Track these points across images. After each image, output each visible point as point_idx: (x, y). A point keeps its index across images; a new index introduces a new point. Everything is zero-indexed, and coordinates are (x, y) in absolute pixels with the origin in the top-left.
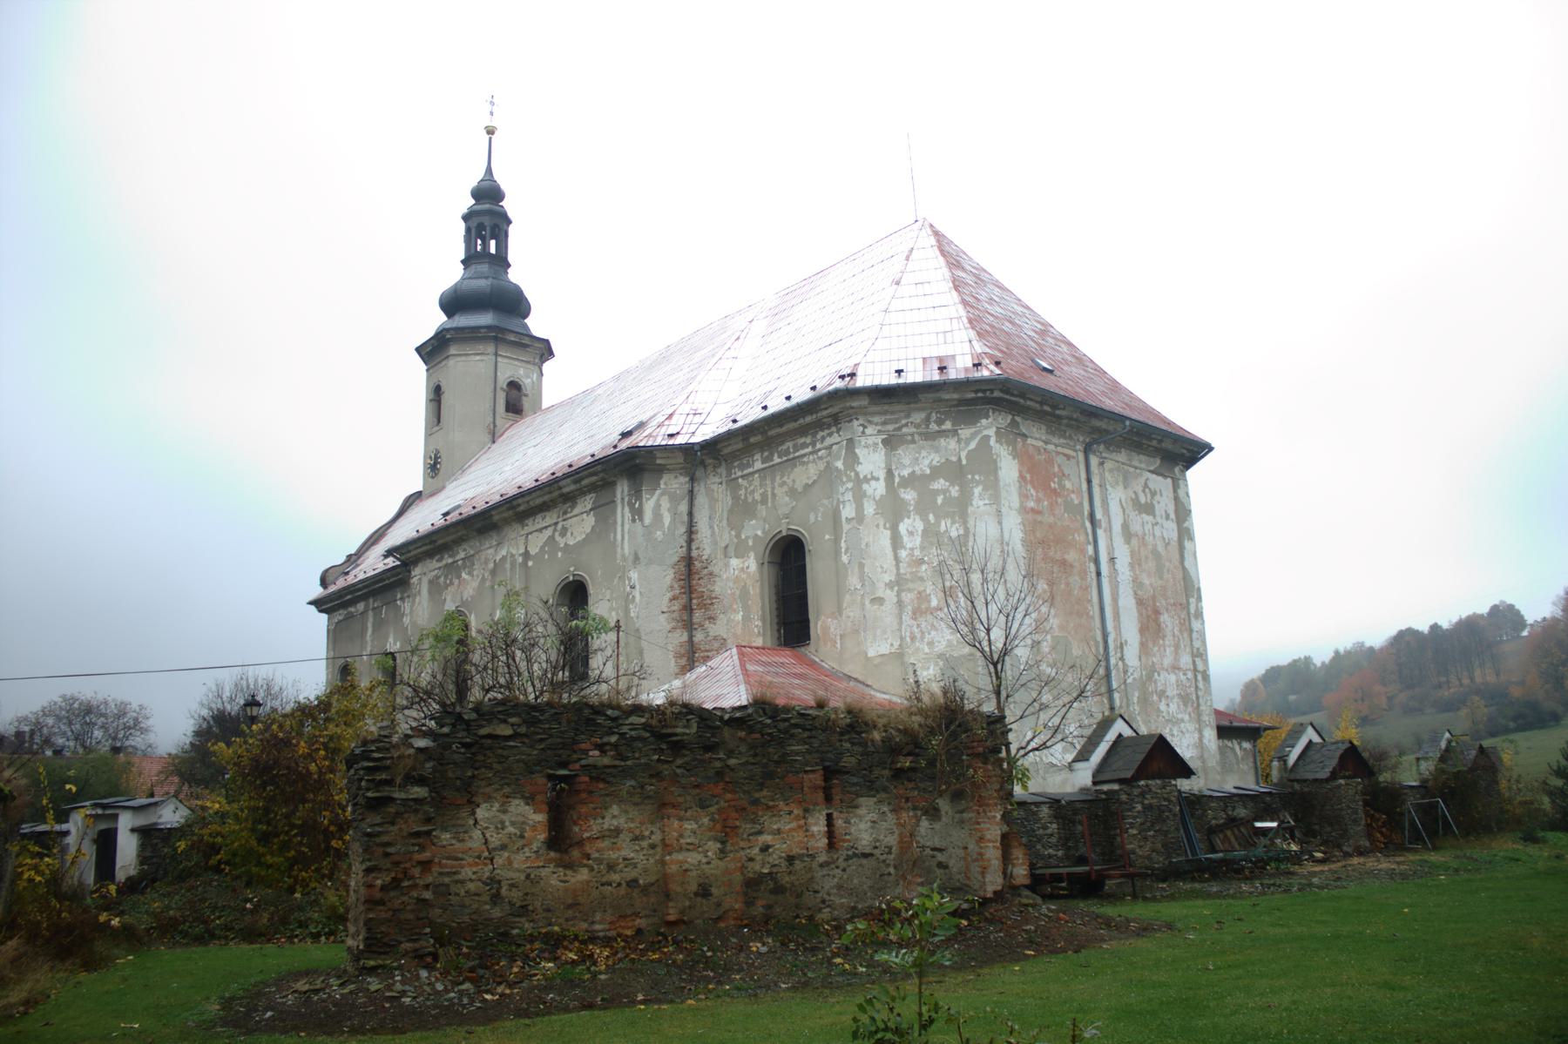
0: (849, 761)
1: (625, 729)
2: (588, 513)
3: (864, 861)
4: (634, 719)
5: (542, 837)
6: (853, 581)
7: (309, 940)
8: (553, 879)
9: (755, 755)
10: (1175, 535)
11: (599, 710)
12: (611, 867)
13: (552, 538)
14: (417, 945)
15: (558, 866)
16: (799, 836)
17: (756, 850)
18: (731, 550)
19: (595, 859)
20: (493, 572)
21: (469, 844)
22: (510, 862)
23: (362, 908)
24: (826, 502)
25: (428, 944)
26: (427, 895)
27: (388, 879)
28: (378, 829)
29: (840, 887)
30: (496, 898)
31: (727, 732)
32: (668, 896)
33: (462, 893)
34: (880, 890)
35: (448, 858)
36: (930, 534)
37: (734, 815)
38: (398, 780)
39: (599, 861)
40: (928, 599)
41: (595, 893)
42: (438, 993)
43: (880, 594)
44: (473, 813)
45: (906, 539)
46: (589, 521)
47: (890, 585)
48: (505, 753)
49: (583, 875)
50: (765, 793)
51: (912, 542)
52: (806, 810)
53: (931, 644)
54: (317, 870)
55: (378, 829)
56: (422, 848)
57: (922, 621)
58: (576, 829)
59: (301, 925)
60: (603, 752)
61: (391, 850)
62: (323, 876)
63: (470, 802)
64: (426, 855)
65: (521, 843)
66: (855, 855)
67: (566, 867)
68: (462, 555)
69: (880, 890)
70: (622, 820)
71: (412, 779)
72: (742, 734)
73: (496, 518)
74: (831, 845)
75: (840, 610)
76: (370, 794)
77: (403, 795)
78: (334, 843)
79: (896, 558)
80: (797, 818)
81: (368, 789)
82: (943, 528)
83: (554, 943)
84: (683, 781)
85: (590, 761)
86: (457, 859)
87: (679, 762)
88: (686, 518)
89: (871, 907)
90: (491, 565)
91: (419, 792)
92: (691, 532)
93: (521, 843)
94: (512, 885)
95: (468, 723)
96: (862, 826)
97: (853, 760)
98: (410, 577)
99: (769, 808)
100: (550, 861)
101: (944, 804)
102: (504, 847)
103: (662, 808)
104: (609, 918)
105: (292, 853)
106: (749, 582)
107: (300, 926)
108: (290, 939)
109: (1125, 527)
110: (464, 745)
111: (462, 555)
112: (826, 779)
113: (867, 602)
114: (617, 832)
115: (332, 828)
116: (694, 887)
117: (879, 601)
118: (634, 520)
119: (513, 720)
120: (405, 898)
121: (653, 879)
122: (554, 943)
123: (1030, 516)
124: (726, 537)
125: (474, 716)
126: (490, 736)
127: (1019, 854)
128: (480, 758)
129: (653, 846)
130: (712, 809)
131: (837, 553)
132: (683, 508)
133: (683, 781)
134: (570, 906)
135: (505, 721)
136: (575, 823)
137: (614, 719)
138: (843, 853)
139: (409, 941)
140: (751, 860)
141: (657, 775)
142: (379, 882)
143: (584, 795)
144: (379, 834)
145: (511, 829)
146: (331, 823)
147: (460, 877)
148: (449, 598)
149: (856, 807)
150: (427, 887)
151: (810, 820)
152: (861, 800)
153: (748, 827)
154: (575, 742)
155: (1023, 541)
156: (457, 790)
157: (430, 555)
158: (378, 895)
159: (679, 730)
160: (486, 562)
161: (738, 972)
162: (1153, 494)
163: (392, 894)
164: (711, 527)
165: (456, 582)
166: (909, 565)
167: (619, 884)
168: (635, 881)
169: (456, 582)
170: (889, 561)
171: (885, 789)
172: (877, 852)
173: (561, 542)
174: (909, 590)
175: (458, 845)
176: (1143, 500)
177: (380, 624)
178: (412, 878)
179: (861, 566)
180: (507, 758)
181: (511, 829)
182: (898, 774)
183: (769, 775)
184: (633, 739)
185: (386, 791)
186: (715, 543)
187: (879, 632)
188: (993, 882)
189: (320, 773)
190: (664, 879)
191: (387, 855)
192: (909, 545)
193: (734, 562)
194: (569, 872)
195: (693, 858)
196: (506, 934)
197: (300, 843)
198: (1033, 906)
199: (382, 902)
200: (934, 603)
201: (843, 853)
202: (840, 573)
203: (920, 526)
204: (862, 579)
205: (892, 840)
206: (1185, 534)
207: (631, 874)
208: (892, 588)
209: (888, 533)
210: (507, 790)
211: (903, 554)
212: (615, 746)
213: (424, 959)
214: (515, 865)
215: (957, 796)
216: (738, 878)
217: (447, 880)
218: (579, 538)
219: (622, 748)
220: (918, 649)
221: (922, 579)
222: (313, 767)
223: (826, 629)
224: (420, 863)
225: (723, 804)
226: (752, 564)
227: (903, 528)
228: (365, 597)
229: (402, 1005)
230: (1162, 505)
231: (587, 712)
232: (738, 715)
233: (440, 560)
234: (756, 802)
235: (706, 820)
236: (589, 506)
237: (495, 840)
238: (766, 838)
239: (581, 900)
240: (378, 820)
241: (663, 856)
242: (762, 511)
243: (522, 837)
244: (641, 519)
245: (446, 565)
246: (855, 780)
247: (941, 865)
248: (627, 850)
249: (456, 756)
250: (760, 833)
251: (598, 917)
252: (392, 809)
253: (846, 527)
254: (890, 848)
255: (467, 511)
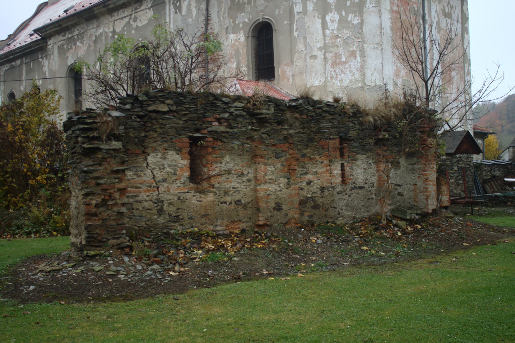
0: (352, 134)
1: (232, 110)
2: (149, 9)
3: (360, 191)
4: (237, 104)
5: (187, 174)
6: (300, 46)
7: (25, 237)
8: (193, 200)
9: (304, 128)
10: (459, 30)
11: (217, 97)
12: (226, 193)
13: (129, 22)
14: (119, 241)
15: (196, 192)
16: (327, 176)
17: (304, 184)
18: (230, 29)
19: (218, 188)
20: (95, 42)
21: (144, 178)
22: (168, 189)
23: (83, 218)
24: (285, 3)
25: (125, 241)
26: (124, 210)
27: (100, 200)
28: (90, 168)
29: (347, 205)
30: (160, 211)
31: (288, 115)
32: (258, 209)
33: (141, 209)
34: (368, 207)
35: (131, 187)
36: (343, 22)
37: (295, 163)
38: (104, 137)
39: (219, 189)
40: (340, 57)
41: (217, 208)
42: (139, 271)
43: (315, 53)
44: (146, 159)
45: (329, 24)
46: (150, 13)
47: (320, 49)
48: (164, 122)
49: (211, 197)
50: (308, 150)
51: (333, 26)
52: (330, 161)
53: (341, 81)
54: (22, 197)
55: (90, 168)
56: (121, 180)
57: (336, 68)
58: (205, 170)
59: (19, 227)
60: (220, 123)
61: (101, 181)
62: (26, 200)
63: (144, 152)
64: (122, 185)
65: (175, 177)
66: (355, 187)
67: (200, 192)
68: (77, 32)
69: (368, 207)
70: (232, 165)
71: (113, 136)
72: (297, 115)
73: (96, 12)
74: (343, 182)
75: (292, 62)
76: (85, 146)
77: (107, 147)
78: (30, 182)
79: (324, 34)
80: (326, 166)
81: (83, 143)
82: (349, 19)
83: (198, 238)
84: (267, 142)
85: (213, 128)
86: (137, 188)
87: (263, 130)
88: (205, 12)
89: (363, 217)
90: (94, 38)
91: (116, 145)
92: (207, 20)
93: (175, 177)
94: (170, 204)
95: (141, 102)
96: (359, 171)
97: (354, 133)
98: (47, 45)
99: (311, 159)
100: (191, 189)
101: (402, 161)
102: (164, 180)
103: (254, 157)
104: (225, 223)
105: (6, 188)
106: (240, 47)
107: (18, 229)
108: (14, 235)
109: (438, 24)
110: (139, 117)
111: (77, 32)
112: (341, 144)
113: (308, 57)
114: (229, 172)
115: (29, 173)
116: (273, 205)
117: (314, 57)
118: (176, 13)
119: (168, 102)
120: (110, 212)
121: (249, 200)
122: (198, 238)
123: (394, 15)
124: (227, 23)
125: (145, 98)
126: (155, 111)
127: (444, 188)
128: (149, 125)
129: (249, 181)
130: (283, 159)
131: (291, 31)
132: (203, 6)
133: (267, 142)
134: (203, 216)
135: (163, 102)
136: (205, 166)
137: (226, 103)
138: (349, 186)
139: (114, 238)
140: (302, 189)
141: (251, 138)
142: (94, 202)
143: (210, 150)
144: (91, 172)
145: (168, 169)
146: (28, 170)
147: (139, 199)
148: (70, 56)
149: (356, 160)
150: (123, 205)
151: (333, 167)
152: (359, 156)
153: (299, 170)
154: (205, 117)
155: (392, 28)
156: (136, 144)
157: (58, 33)
158: (94, 210)
159: (264, 111)
160: (91, 36)
161: (313, 254)
162: (452, 8)
163: (101, 209)
164: (219, 17)
165: (74, 47)
166: (331, 38)
167: (231, 203)
168: (239, 201)
169: (74, 47)
170: (320, 36)
171: (371, 151)
172: (366, 186)
173: (134, 25)
174: (331, 52)
175: (137, 179)
176: (447, 11)
177: (29, 71)
178: (115, 199)
179: (305, 38)
180: (165, 125)
181: (168, 169)
182: (379, 142)
183: (311, 140)
184: (238, 116)
185: (96, 144)
186: (221, 26)
187: (313, 74)
188: (432, 204)
189: (21, 142)
190: (256, 200)
191: (98, 184)
192: (331, 28)
193: (232, 36)
194: (202, 196)
195: (272, 187)
196: (167, 233)
197: (11, 182)
198: (451, 218)
199: (96, 215)
200: (344, 59)
201: (349, 186)
202: (293, 42)
203: (337, 17)
204: (305, 46)
205: (374, 179)
206: (465, 30)
207: (237, 197)
208: (321, 51)
209: (320, 21)
210: (165, 145)
211: (328, 32)
212: (227, 120)
213: (125, 250)
214: (172, 191)
215: (409, 155)
216: (296, 200)
217: (131, 200)
218: (144, 23)
219: (231, 121)
220: (334, 83)
221: (337, 46)
222: (17, 139)
223: (284, 72)
224: (119, 190)
225: (288, 156)
226: (242, 37)
227: (328, 18)
228: (20, 57)
229: (119, 280)
230: (456, 14)
231: (211, 98)
232: (294, 104)
233: (64, 36)
234: (304, 156)
235: (279, 166)
236: (150, 5)
237: (159, 176)
238: (309, 177)
239: (210, 212)
240: (91, 162)
241: (255, 186)
242: (248, 8)
243: (175, 174)
244: (180, 12)
245: (68, 38)
246: (355, 144)
247: (400, 194)
248: (234, 182)
249: (135, 123)
250: (306, 173)
251: (219, 223)
252: (99, 156)
253: (297, 17)
254: (373, 184)
255: (79, 8)
